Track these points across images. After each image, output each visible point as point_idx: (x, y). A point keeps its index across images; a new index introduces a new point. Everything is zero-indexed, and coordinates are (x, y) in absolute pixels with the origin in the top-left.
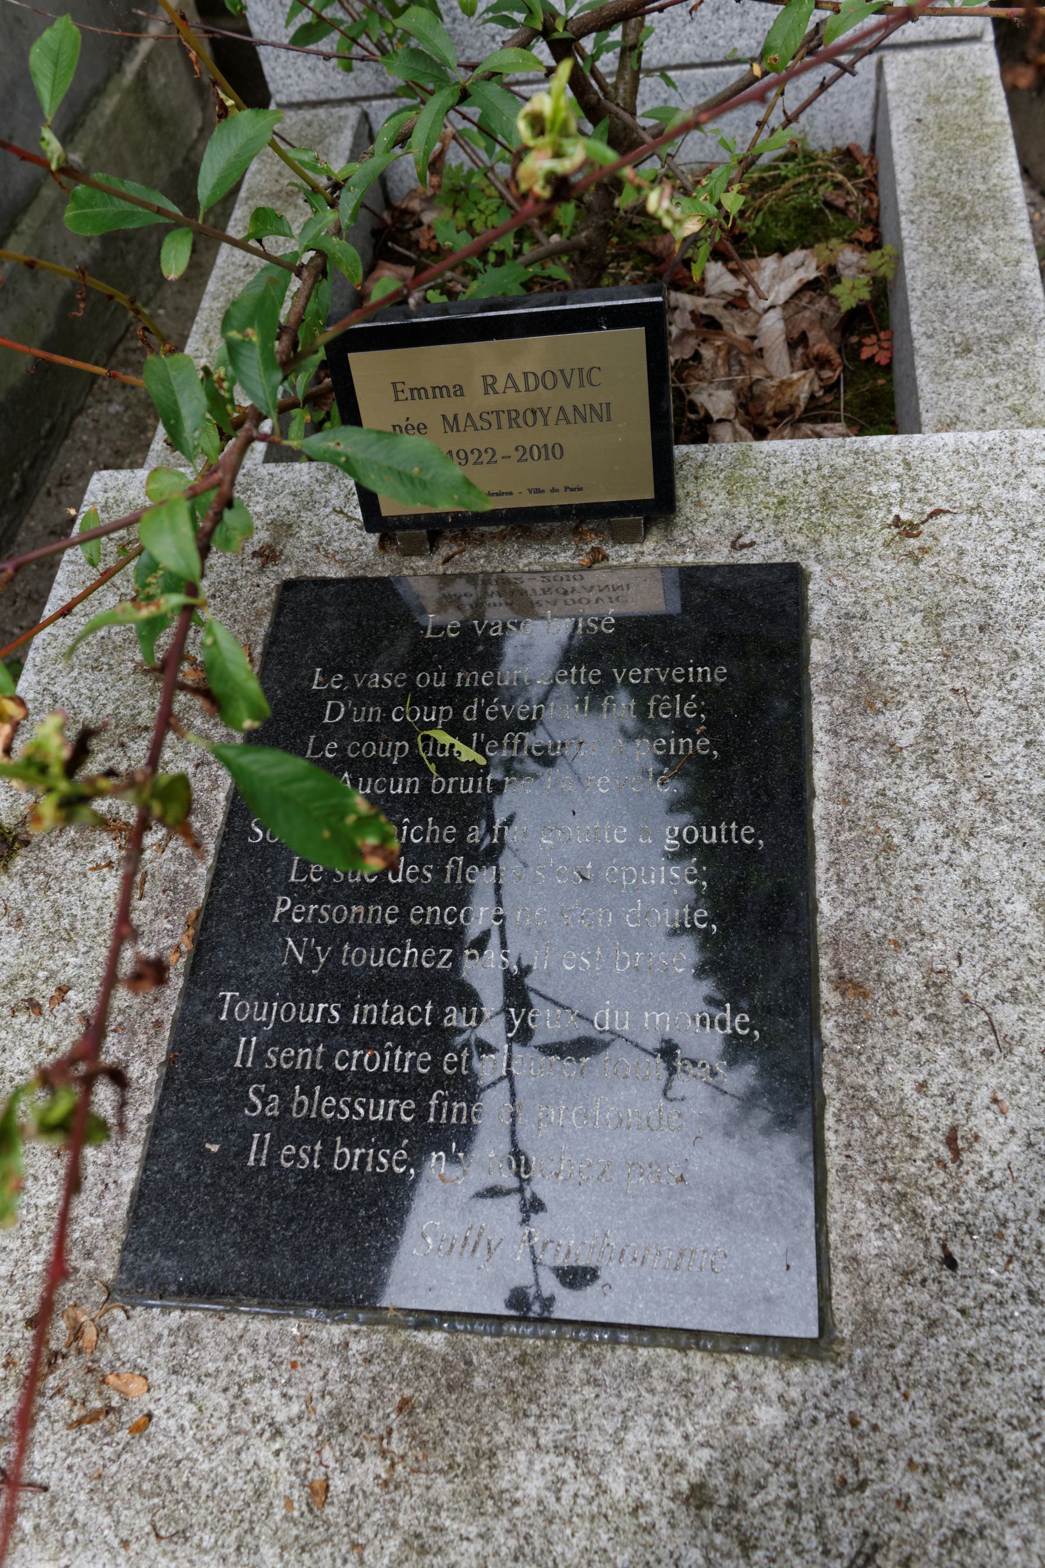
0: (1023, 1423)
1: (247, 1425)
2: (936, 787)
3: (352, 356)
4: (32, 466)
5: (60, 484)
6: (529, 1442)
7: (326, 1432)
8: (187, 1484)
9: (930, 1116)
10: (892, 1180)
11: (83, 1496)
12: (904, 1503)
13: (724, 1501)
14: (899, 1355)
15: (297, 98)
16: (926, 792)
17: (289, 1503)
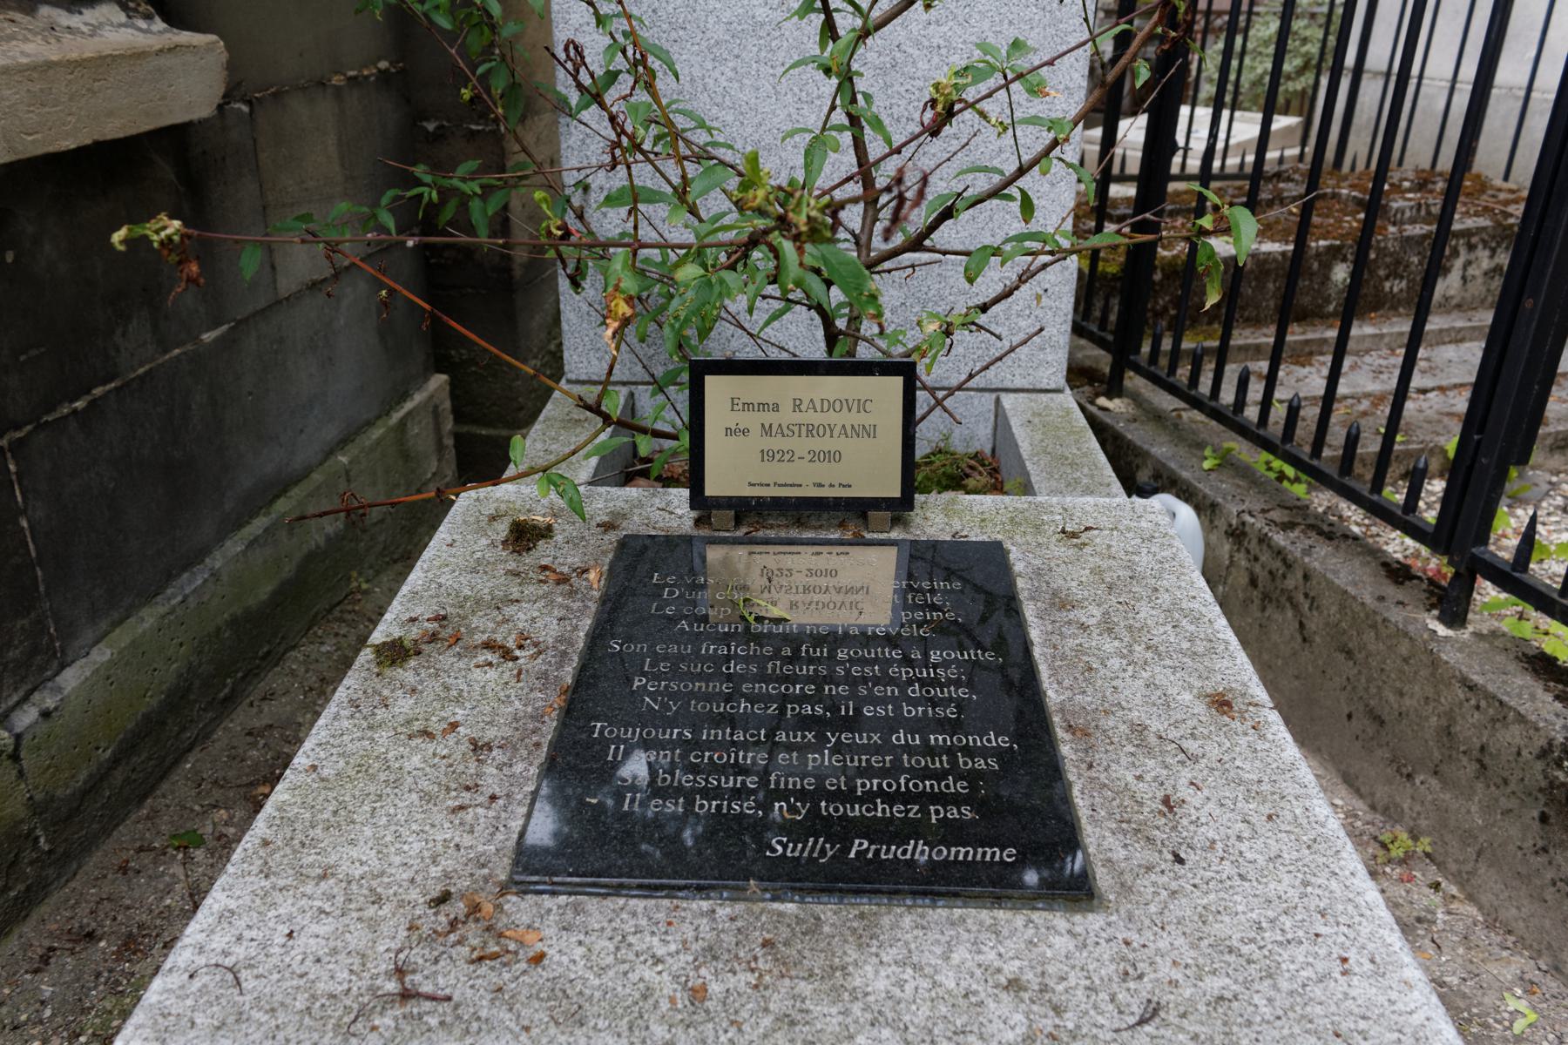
0: (1252, 941)
1: (631, 956)
2: (1116, 643)
3: (707, 378)
4: (243, 678)
5: (264, 699)
6: (875, 960)
7: (701, 959)
8: (581, 993)
9: (1149, 793)
10: (1129, 822)
11: (484, 1003)
12: (1174, 983)
13: (1037, 988)
14: (1153, 908)
15: (584, 377)
16: (1110, 646)
17: (672, 1000)
